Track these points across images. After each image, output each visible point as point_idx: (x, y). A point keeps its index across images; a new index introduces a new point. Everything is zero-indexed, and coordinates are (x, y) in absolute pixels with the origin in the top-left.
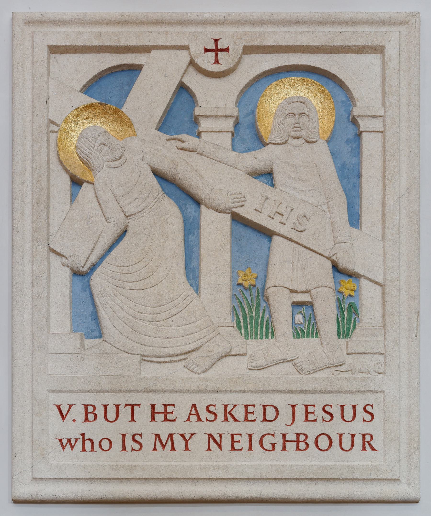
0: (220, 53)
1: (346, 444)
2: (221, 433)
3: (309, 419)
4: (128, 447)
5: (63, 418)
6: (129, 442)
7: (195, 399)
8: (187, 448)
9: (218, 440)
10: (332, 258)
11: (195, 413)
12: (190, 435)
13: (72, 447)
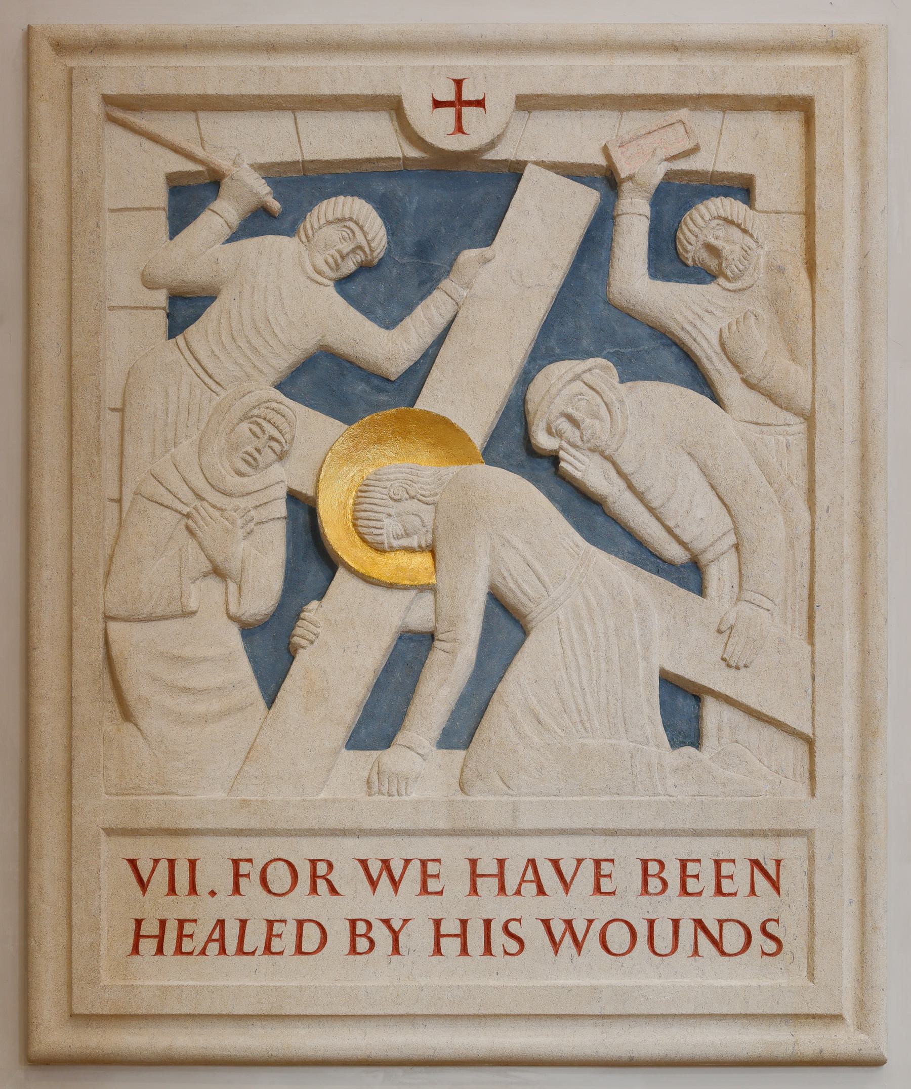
0: (465, 110)
1: (663, 942)
2: (243, 918)
3: (603, 889)
4: (496, 948)
5: (143, 885)
6: (499, 939)
7: (282, 847)
8: (396, 950)
9: (772, 873)
10: (698, 557)
11: (533, 879)
12: (401, 922)
13: (395, 884)
